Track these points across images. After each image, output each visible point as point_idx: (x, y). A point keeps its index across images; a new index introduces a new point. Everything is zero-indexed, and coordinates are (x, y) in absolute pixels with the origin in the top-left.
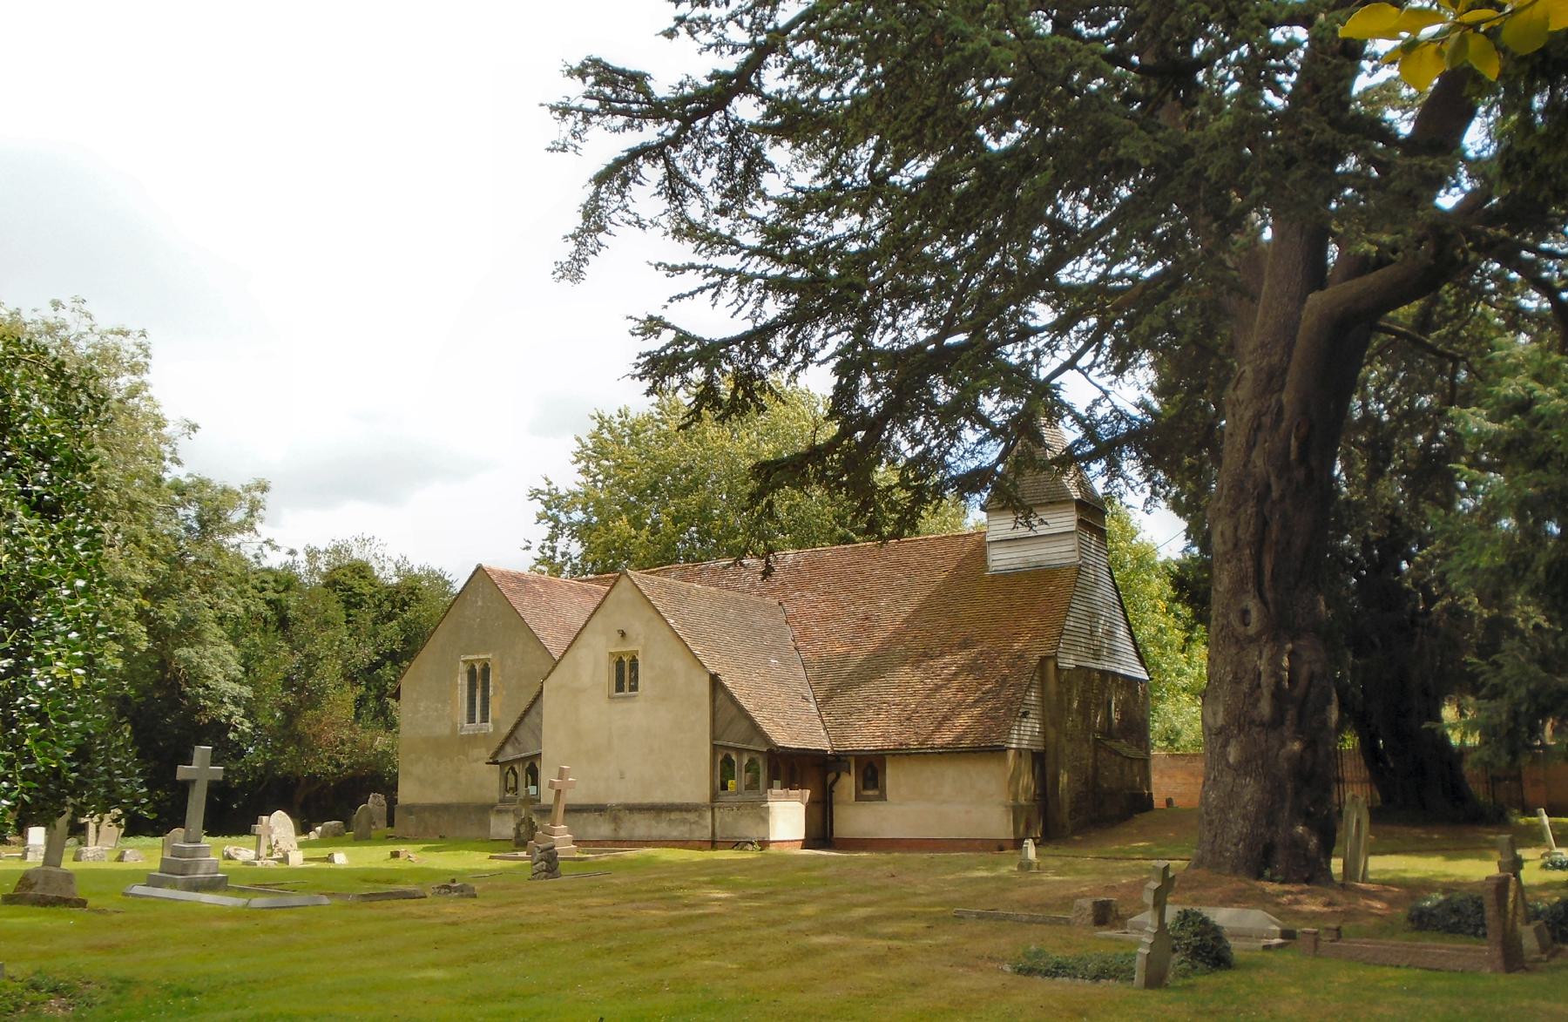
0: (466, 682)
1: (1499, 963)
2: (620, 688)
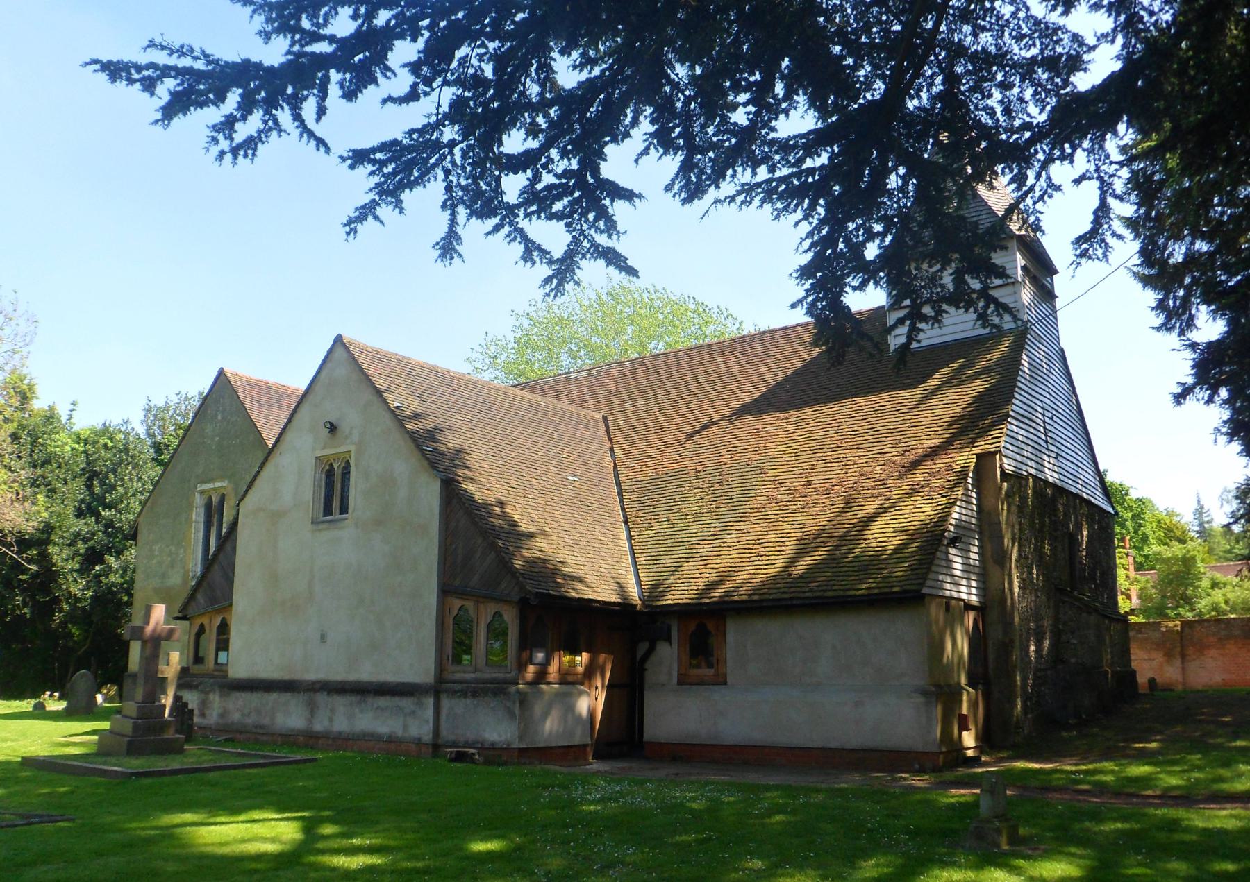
0: (202, 519)
1: (538, 368)
2: (328, 511)
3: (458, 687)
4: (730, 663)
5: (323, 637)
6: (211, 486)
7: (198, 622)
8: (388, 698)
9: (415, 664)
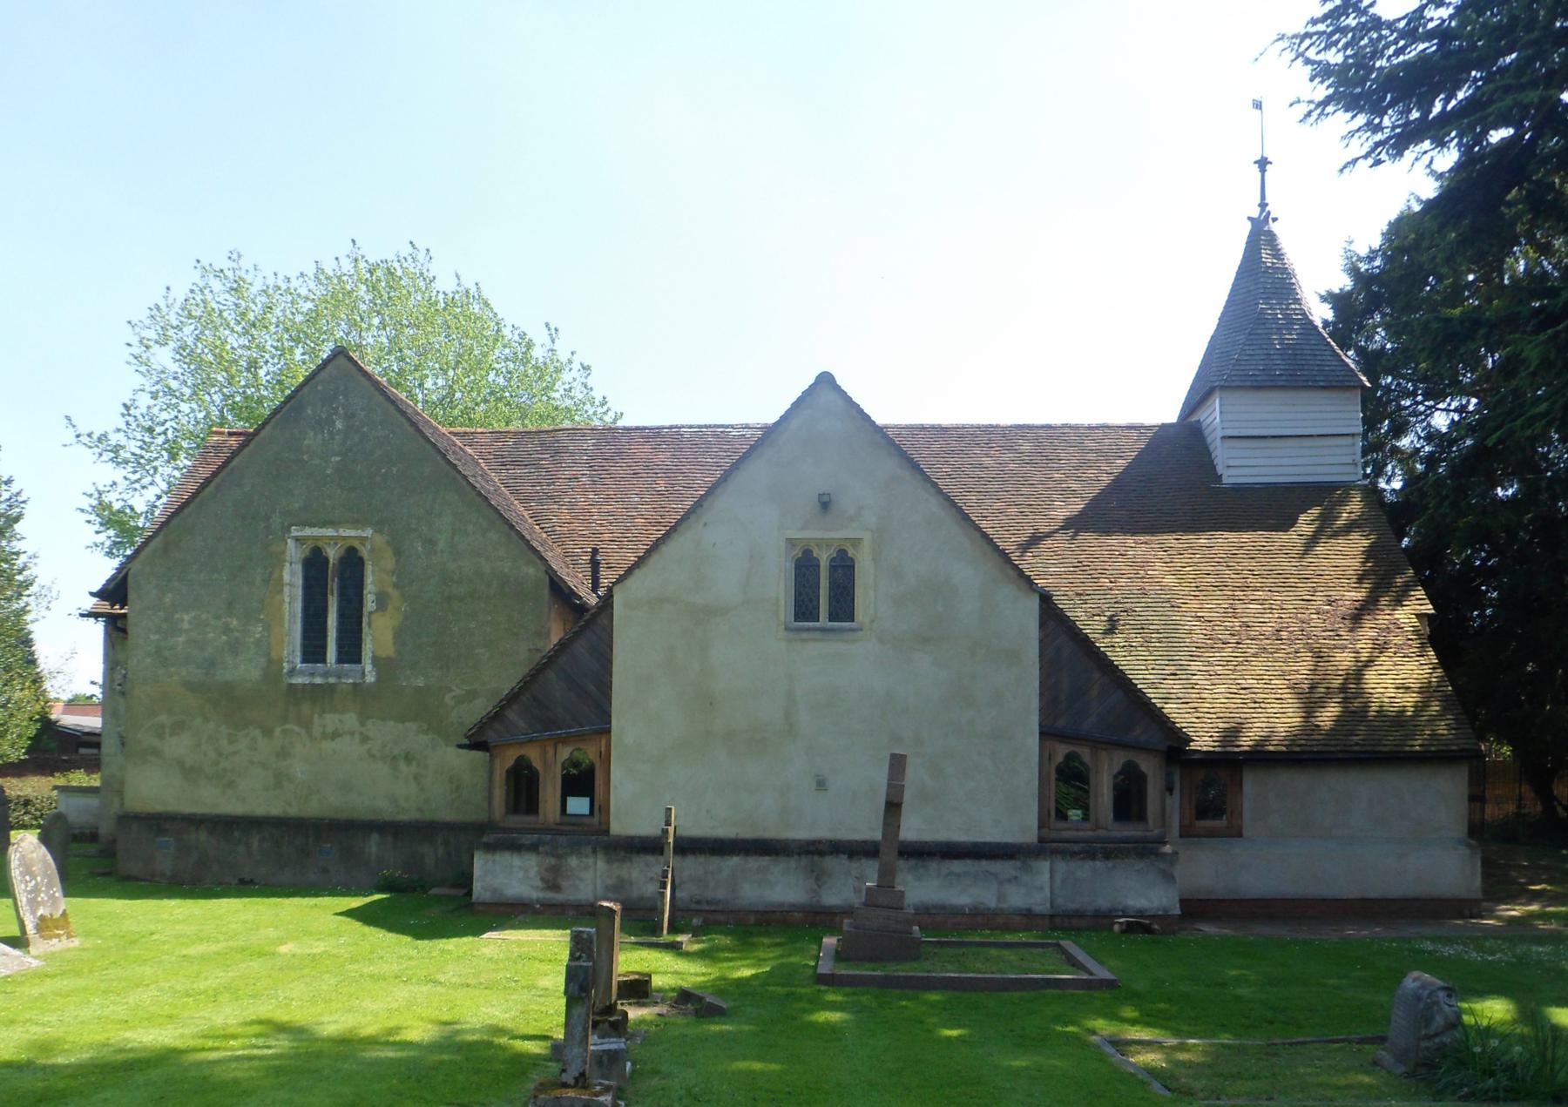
3: (1076, 848)
4: (1247, 815)
5: (821, 784)
6: (330, 532)
7: (509, 758)
8: (969, 862)
9: (1021, 825)
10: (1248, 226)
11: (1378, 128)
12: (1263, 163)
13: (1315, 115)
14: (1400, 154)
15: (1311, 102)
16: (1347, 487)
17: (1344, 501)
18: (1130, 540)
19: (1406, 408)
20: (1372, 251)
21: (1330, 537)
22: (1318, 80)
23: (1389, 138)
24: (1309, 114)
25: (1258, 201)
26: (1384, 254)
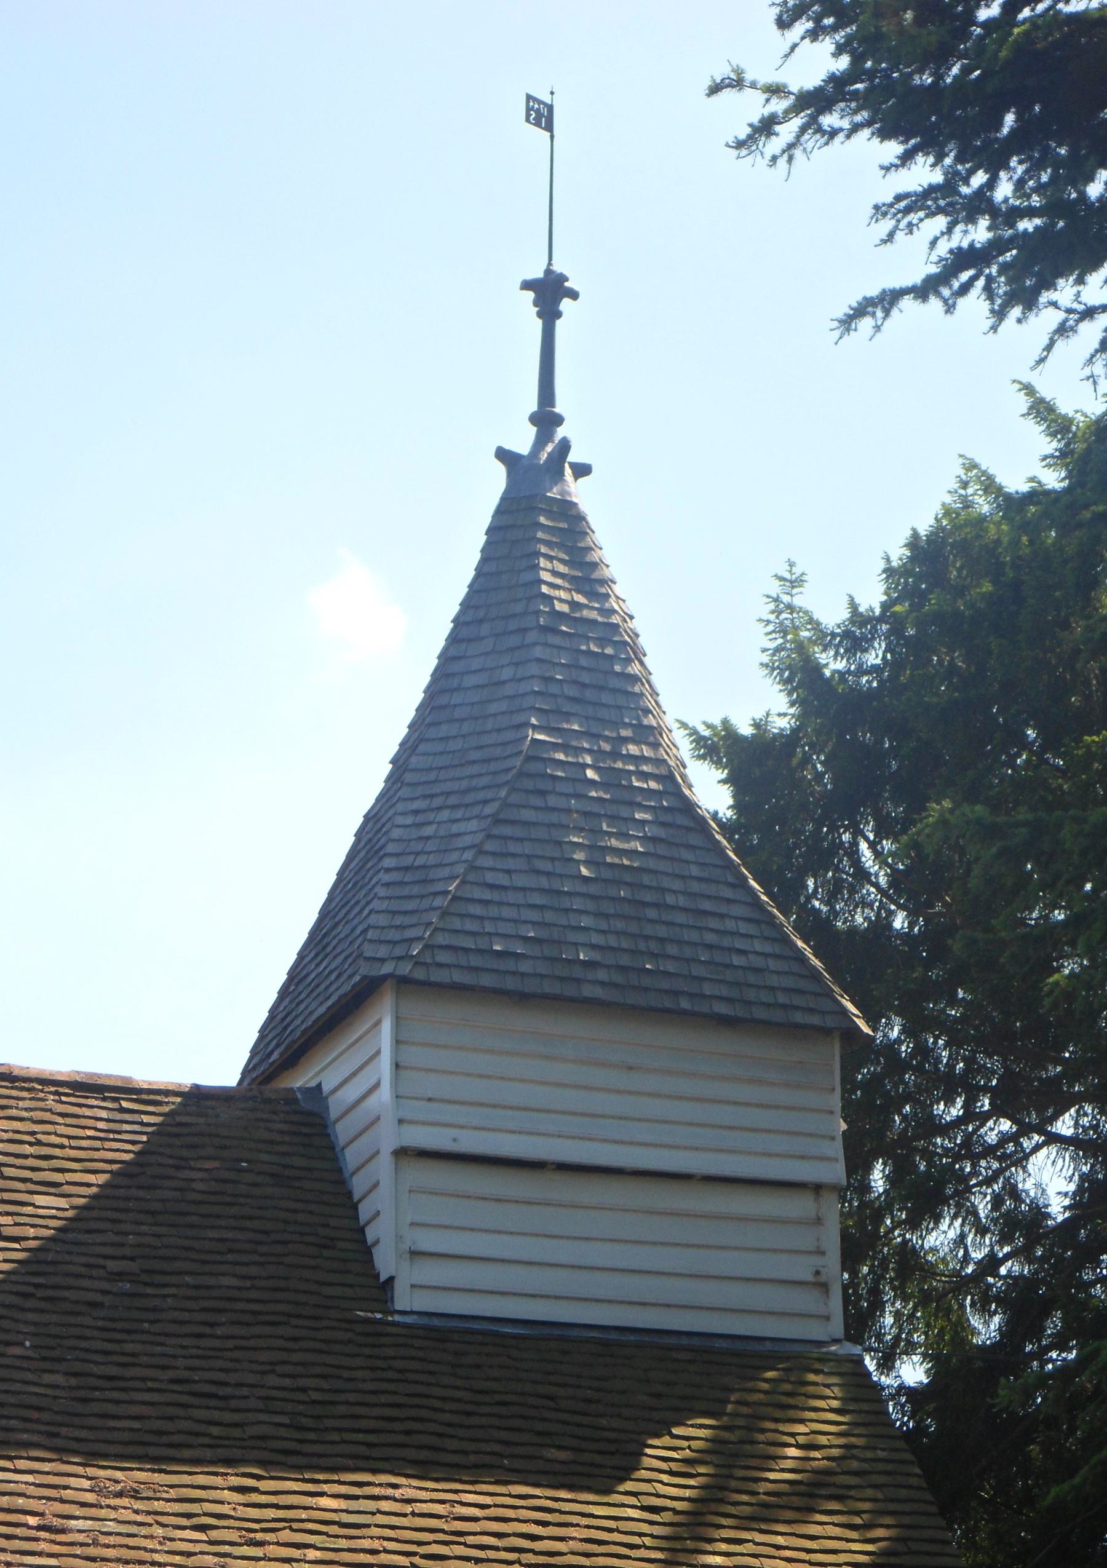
10: (497, 479)
11: (979, 205)
12: (549, 293)
13: (787, 131)
14: (1028, 300)
15: (775, 90)
16: (796, 1360)
17: (787, 1405)
18: (80, 1480)
19: (946, 1129)
20: (857, 617)
21: (747, 1522)
22: (803, 25)
23: (996, 247)
24: (766, 127)
25: (532, 405)
26: (897, 629)
